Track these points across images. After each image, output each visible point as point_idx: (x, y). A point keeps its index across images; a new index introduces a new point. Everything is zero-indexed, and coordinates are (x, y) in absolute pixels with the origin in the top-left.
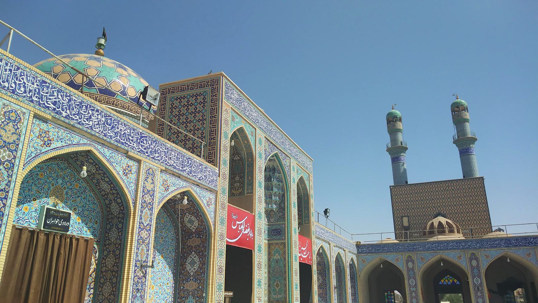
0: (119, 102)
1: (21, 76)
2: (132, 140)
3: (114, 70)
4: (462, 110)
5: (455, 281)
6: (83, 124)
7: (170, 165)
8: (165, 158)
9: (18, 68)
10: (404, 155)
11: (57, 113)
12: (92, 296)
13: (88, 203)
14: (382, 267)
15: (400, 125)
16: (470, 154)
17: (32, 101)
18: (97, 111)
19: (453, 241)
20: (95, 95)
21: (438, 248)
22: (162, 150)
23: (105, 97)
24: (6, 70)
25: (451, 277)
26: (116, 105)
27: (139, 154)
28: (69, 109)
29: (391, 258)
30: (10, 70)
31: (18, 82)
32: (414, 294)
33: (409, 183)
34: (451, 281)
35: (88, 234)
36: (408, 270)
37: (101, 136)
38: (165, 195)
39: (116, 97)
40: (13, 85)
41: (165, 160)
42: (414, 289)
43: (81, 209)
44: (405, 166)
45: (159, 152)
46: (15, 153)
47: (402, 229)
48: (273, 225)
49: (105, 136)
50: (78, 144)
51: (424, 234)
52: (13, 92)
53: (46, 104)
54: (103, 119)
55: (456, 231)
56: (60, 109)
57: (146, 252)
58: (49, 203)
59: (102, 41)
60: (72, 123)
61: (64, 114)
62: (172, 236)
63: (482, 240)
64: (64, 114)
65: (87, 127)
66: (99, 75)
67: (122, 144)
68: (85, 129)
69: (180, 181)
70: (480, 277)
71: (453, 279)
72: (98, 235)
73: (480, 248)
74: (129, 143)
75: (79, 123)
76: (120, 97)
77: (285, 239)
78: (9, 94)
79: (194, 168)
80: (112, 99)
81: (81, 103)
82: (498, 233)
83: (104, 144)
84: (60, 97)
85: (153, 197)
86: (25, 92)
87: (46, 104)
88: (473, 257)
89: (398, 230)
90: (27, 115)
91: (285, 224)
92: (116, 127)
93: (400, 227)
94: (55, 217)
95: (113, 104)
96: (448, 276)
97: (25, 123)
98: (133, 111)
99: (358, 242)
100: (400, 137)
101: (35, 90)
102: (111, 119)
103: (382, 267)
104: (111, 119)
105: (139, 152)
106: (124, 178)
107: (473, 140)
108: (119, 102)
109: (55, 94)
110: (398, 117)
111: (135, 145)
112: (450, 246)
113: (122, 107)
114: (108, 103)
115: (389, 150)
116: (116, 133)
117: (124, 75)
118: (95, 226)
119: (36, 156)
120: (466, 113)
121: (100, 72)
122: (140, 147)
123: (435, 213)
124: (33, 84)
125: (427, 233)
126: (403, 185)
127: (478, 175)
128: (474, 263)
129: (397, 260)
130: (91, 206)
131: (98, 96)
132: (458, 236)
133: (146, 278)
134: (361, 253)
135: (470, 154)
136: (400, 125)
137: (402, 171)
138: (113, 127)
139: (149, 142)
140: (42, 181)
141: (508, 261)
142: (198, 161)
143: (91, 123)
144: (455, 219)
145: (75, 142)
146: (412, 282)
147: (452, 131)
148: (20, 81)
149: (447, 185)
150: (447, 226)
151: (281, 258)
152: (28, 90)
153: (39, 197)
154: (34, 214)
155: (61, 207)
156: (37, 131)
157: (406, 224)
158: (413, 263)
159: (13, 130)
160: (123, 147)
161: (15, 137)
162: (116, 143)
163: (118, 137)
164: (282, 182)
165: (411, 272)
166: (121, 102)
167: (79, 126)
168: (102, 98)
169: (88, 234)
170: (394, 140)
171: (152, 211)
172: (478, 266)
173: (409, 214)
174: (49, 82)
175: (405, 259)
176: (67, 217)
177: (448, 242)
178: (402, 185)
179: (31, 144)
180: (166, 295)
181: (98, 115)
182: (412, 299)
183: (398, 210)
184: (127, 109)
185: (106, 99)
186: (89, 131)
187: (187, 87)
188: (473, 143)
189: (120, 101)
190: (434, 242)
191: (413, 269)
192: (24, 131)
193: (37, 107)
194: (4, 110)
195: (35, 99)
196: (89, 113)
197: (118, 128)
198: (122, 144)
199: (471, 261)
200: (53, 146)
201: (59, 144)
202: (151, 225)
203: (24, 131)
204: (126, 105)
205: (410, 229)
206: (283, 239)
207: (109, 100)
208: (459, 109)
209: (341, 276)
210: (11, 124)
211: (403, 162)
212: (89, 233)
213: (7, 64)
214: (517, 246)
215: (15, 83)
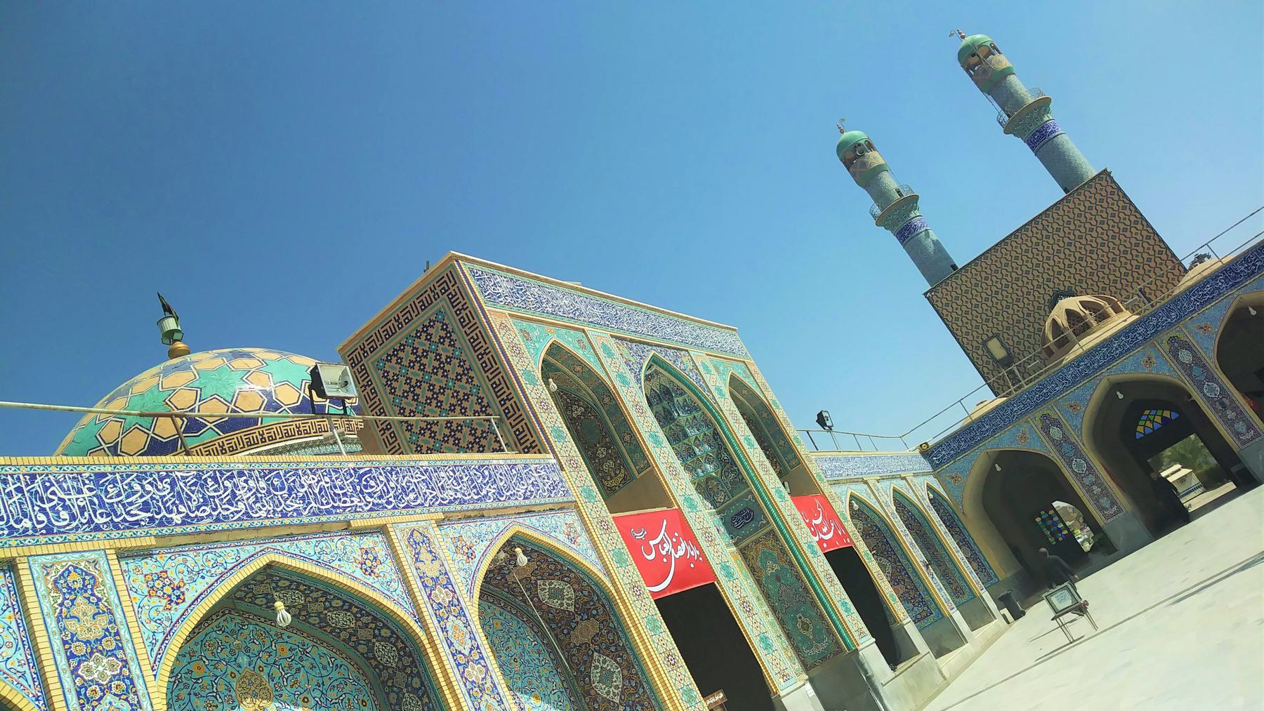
0: (273, 428)
1: (46, 489)
3: (227, 370)
4: (987, 56)
5: (1167, 414)
6: (226, 517)
7: (450, 502)
8: (431, 494)
9: (33, 477)
10: (918, 214)
11: (161, 524)
14: (999, 469)
15: (875, 158)
16: (1051, 136)
17: (97, 528)
18: (241, 474)
19: (1116, 336)
20: (216, 442)
22: (416, 481)
23: (239, 435)
25: (1153, 412)
26: (270, 438)
27: (374, 514)
29: (1006, 440)
30: (19, 490)
31: (47, 506)
32: (1096, 490)
33: (960, 267)
34: (1158, 419)
36: (1058, 445)
39: (261, 424)
40: (42, 517)
41: (434, 497)
42: (1091, 478)
44: (933, 236)
45: (411, 488)
46: (120, 654)
47: (998, 367)
49: (284, 515)
50: (239, 564)
51: (1050, 352)
55: (1110, 311)
56: (164, 513)
59: (171, 324)
61: (177, 518)
62: (533, 644)
63: (1176, 300)
64: (177, 518)
65: (239, 519)
70: (1212, 379)
71: (1159, 412)
73: (1179, 318)
75: (218, 520)
76: (271, 419)
78: (43, 539)
79: (501, 480)
80: (256, 431)
81: (198, 477)
82: (1200, 267)
84: (148, 488)
86: (73, 517)
88: (1177, 345)
89: (990, 376)
90: (102, 561)
91: (751, 492)
92: (297, 484)
93: (990, 367)
95: (263, 440)
96: (1147, 412)
98: (312, 431)
99: (921, 445)
100: (890, 182)
102: (278, 476)
103: (999, 469)
104: (278, 476)
106: (370, 580)
107: (1043, 105)
108: (273, 428)
110: (862, 142)
111: (356, 500)
112: (1117, 349)
113: (286, 437)
114: (252, 443)
115: (881, 221)
116: (303, 498)
119: (167, 635)
120: (998, 57)
121: (201, 389)
123: (1047, 297)
124: (80, 491)
125: (1054, 348)
126: (951, 277)
127: (1092, 171)
128: (1185, 356)
129: (1023, 437)
130: (335, 675)
131: (224, 440)
132: (1121, 320)
134: (941, 464)
135: (1051, 136)
136: (875, 158)
137: (931, 248)
138: (290, 490)
139: (382, 478)
141: (1253, 312)
143: (241, 506)
144: (1096, 288)
146: (1079, 466)
147: (988, 111)
148: (51, 500)
149: (1040, 227)
150: (1087, 312)
151: (782, 568)
152: (76, 510)
157: (999, 353)
158: (1058, 424)
159: (92, 610)
160: (332, 518)
161: (103, 621)
162: (315, 519)
163: (313, 504)
164: (697, 409)
165: (1066, 448)
166: (277, 426)
167: (220, 526)
168: (233, 441)
170: (879, 195)
171: (465, 616)
172: (1197, 360)
173: (995, 331)
175: (1040, 427)
177: (1106, 343)
178: (948, 279)
183: (967, 333)
184: (299, 434)
185: (244, 438)
186: (246, 524)
187: (396, 324)
188: (1047, 111)
189: (274, 427)
190: (1079, 359)
191: (1065, 438)
193: (114, 534)
194: (51, 578)
195: (99, 520)
196: (226, 488)
197: (303, 486)
198: (328, 512)
199: (1176, 356)
200: (189, 597)
201: (201, 586)
202: (478, 648)
204: (291, 427)
205: (1016, 359)
206: (764, 525)
207: (250, 436)
208: (978, 56)
210: (80, 599)
211: (922, 230)
214: (1253, 273)
215: (43, 510)
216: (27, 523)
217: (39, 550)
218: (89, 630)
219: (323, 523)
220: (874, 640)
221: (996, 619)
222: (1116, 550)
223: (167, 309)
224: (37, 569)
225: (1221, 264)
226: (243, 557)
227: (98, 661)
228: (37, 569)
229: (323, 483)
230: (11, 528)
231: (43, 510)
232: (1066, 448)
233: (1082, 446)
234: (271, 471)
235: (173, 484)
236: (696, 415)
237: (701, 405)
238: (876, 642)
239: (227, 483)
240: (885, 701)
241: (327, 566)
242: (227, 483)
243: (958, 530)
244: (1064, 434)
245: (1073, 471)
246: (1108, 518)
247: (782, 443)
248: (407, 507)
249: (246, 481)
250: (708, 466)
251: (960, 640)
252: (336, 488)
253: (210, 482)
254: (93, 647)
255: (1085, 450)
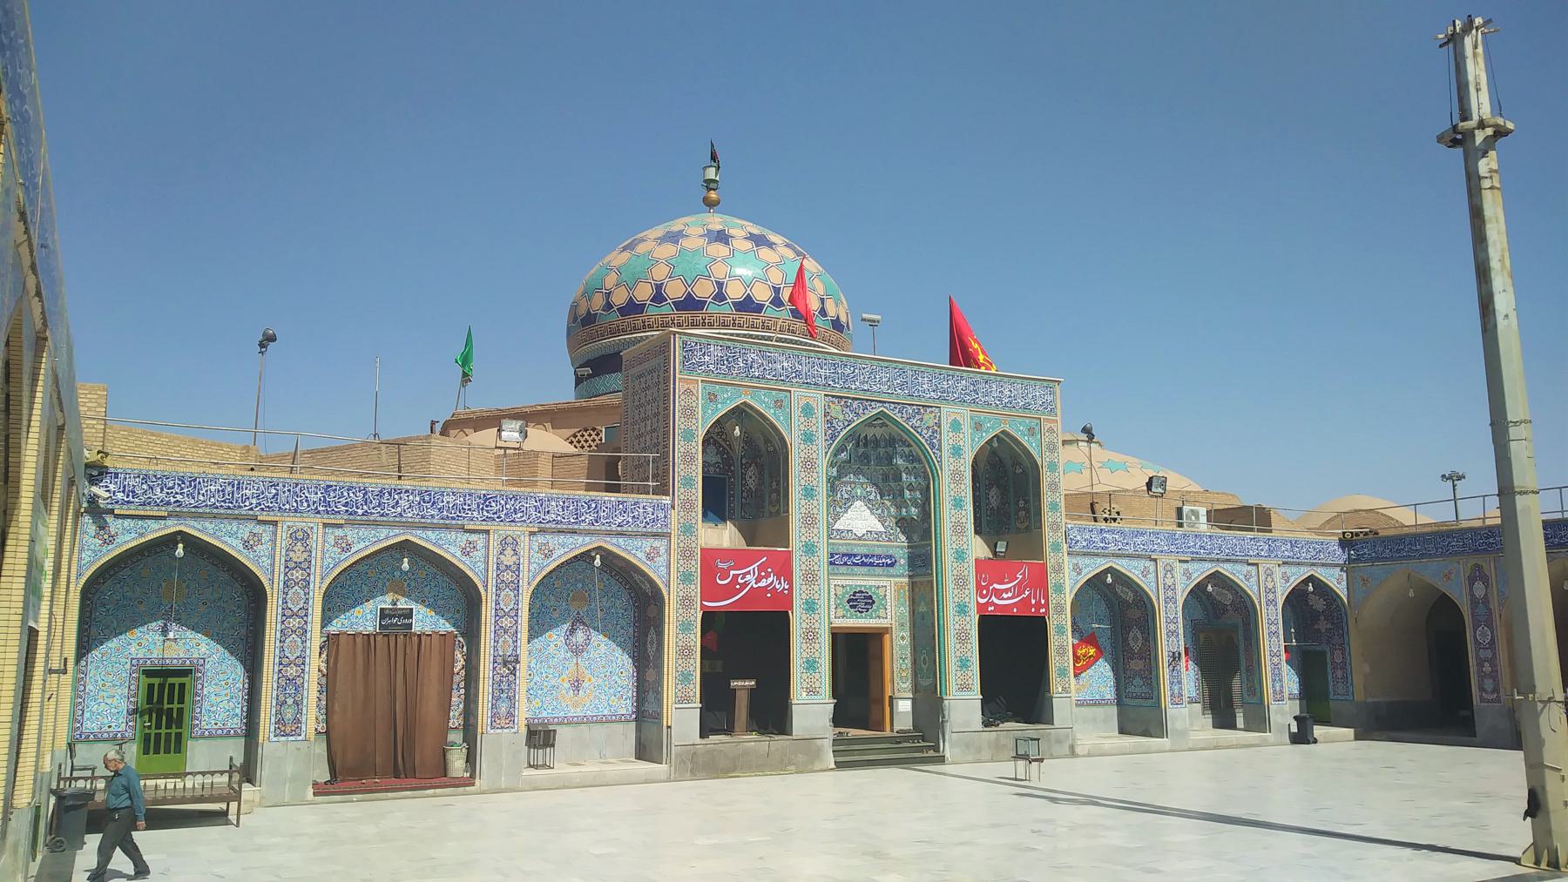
1: (301, 491)
2: (469, 510)
6: (387, 515)
7: (549, 521)
9: (297, 485)
11: (351, 514)
12: (463, 697)
13: (441, 591)
17: (318, 512)
18: (407, 491)
21: (1552, 542)
22: (528, 505)
24: (284, 492)
27: (484, 523)
28: (366, 504)
30: (289, 490)
31: (298, 499)
32: (1487, 668)
35: (445, 627)
36: (1474, 602)
37: (417, 520)
38: (545, 564)
40: (295, 504)
42: (1489, 654)
43: (432, 600)
46: (308, 570)
48: (916, 547)
49: (423, 517)
50: (387, 538)
52: (296, 511)
53: (336, 509)
54: (418, 499)
56: (354, 508)
57: (511, 644)
58: (385, 602)
59: (711, 173)
60: (372, 519)
61: (360, 512)
64: (360, 512)
65: (395, 516)
66: (673, 275)
67: (453, 518)
68: (391, 519)
69: (576, 538)
72: (463, 626)
74: (464, 515)
75: (382, 515)
76: (712, 309)
77: (932, 574)
78: (292, 514)
79: (604, 511)
81: (381, 492)
83: (426, 527)
84: (351, 495)
85: (517, 573)
86: (309, 506)
87: (336, 509)
90: (315, 528)
91: (931, 545)
92: (440, 500)
94: (391, 617)
97: (315, 538)
101: (320, 500)
102: (430, 495)
104: (430, 495)
105: (484, 520)
106: (464, 558)
109: (346, 494)
111: (475, 514)
116: (439, 509)
117: (719, 259)
118: (457, 616)
119: (335, 566)
122: (485, 513)
124: (316, 494)
129: (1448, 577)
130: (448, 593)
133: (515, 675)
134: (1357, 560)
138: (434, 503)
139: (502, 502)
140: (374, 579)
142: (613, 499)
143: (399, 509)
145: (383, 536)
146: (1484, 634)
148: (301, 497)
152: (311, 503)
153: (373, 597)
154: (369, 616)
155: (403, 604)
156: (331, 540)
159: (302, 549)
160: (454, 522)
161: (305, 555)
162: (441, 521)
163: (445, 513)
164: (920, 461)
167: (382, 519)
169: (445, 627)
174: (335, 484)
176: (409, 614)
179: (327, 555)
180: (620, 689)
181: (408, 496)
182: (1483, 680)
186: (397, 519)
187: (701, 321)
191: (1486, 600)
192: (314, 546)
193: (326, 516)
194: (290, 532)
195: (321, 509)
196: (394, 499)
197: (443, 502)
198: (453, 518)
200: (353, 550)
201: (362, 545)
202: (517, 610)
203: (314, 546)
206: (928, 574)
209: (1249, 625)
210: (299, 544)
212: (447, 625)
213: (284, 486)
215: (296, 501)
216: (287, 506)
217: (288, 519)
218: (298, 558)
219: (446, 524)
220: (981, 697)
221: (1270, 732)
222: (1475, 736)
223: (714, 157)
224: (285, 527)
225: (1561, 517)
226: (391, 534)
227: (297, 572)
228: (285, 527)
229: (458, 501)
230: (280, 507)
231: (296, 501)
232: (1481, 609)
233: (1498, 617)
234: (426, 491)
235: (365, 495)
236: (917, 466)
237: (924, 459)
238: (701, 708)
239: (396, 497)
240: (947, 744)
241: (440, 547)
242: (396, 497)
243: (1341, 632)
244: (1486, 595)
245: (1475, 636)
246: (1482, 700)
247: (1037, 504)
248: (512, 521)
249: (408, 496)
250: (913, 509)
251: (729, 730)
252: (465, 504)
253: (386, 495)
254: (298, 565)
255: (1498, 624)
